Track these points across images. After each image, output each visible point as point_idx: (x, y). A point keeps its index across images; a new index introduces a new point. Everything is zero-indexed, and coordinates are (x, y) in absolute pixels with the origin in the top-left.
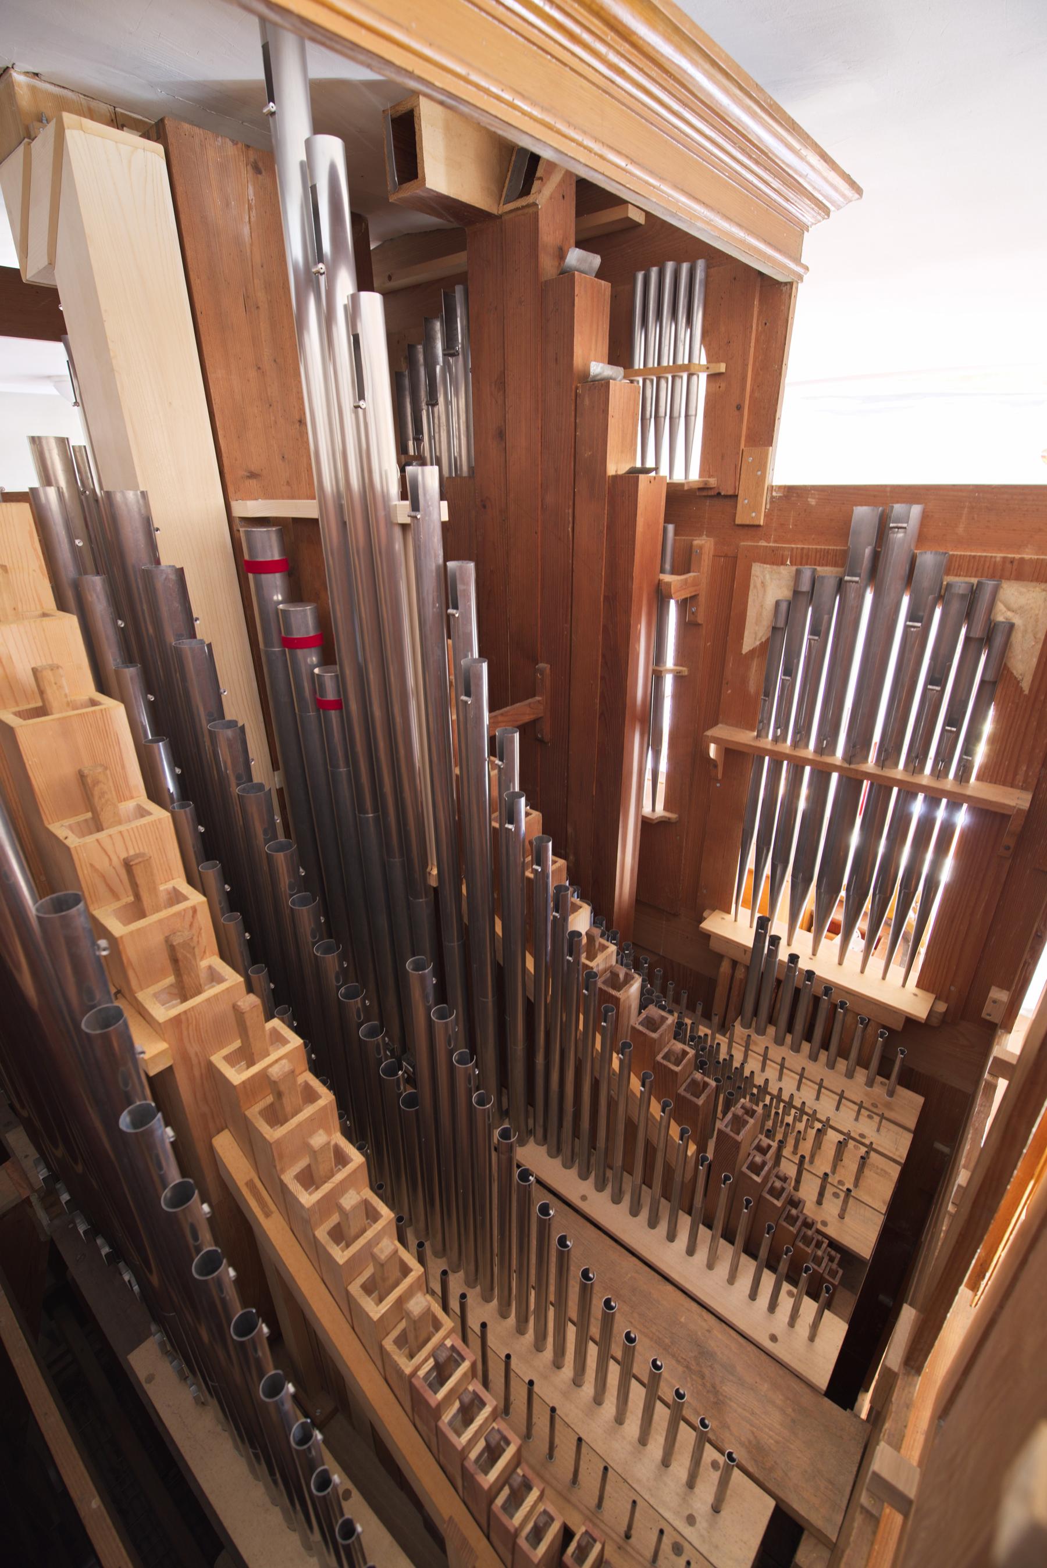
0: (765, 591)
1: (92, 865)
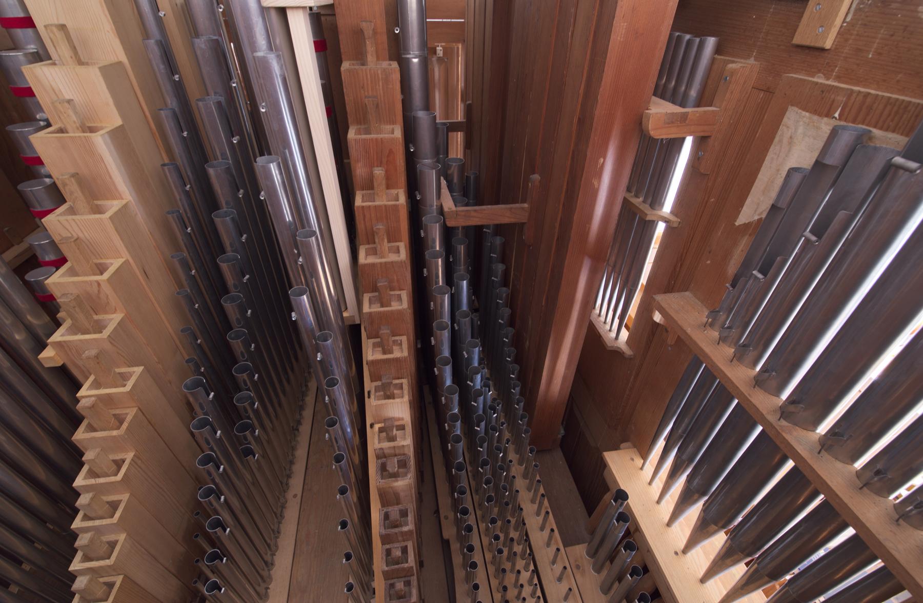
0: (789, 151)
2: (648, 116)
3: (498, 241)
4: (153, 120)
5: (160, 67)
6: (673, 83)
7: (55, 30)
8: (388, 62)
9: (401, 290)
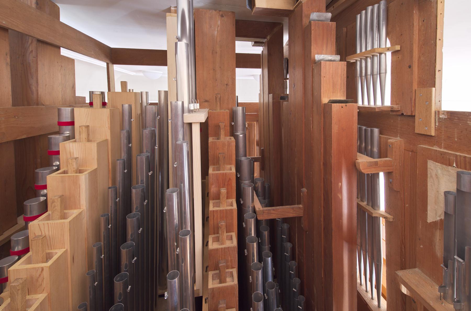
0: (439, 182)
1: (34, 233)
2: (359, 163)
3: (286, 226)
4: (112, 164)
5: (124, 141)
6: (364, 144)
7: (84, 128)
8: (229, 137)
9: (233, 268)
